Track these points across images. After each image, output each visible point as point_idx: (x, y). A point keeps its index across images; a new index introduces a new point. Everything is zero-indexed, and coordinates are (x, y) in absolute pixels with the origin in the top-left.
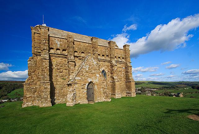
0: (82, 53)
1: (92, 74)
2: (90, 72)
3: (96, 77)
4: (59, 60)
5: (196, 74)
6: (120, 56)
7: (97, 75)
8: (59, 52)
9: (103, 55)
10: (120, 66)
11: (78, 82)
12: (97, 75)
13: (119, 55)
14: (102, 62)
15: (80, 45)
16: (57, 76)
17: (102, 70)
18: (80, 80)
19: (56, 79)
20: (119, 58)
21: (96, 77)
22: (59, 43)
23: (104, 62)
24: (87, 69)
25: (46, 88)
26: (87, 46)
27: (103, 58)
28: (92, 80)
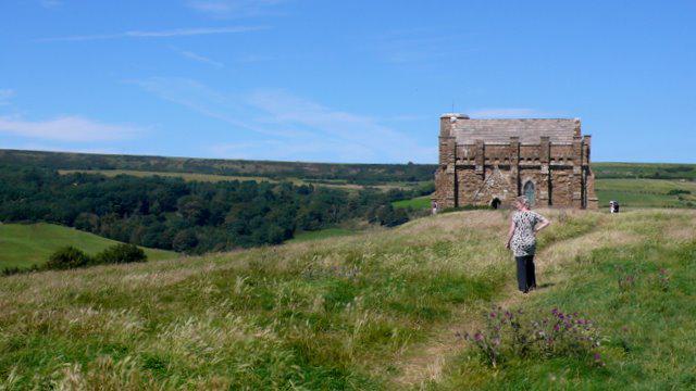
0: (496, 159)
4: (466, 171)
9: (529, 159)
27: (530, 163)
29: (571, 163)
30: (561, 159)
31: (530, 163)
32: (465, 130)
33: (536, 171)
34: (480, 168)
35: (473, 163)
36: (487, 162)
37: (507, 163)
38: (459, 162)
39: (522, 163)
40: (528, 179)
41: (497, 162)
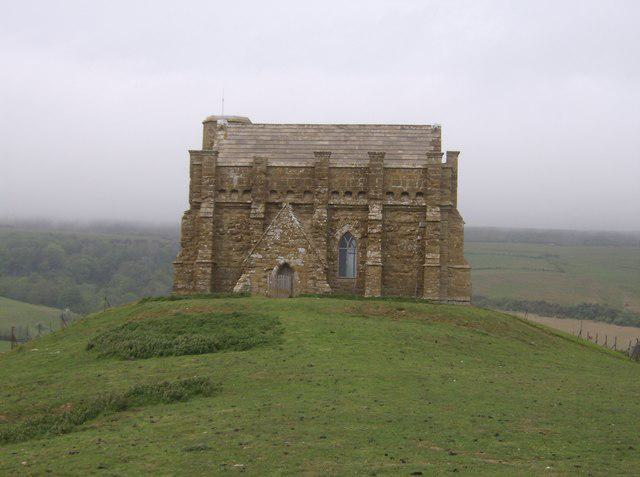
0: (289, 192)
1: (288, 247)
2: (284, 246)
3: (297, 254)
5: (5, 293)
6: (405, 190)
7: (300, 249)
8: (406, 202)
9: (348, 193)
10: (408, 217)
11: (258, 264)
12: (300, 249)
13: (404, 185)
14: (344, 212)
15: (283, 174)
16: (231, 249)
17: (344, 231)
18: (261, 260)
19: (228, 255)
20: (405, 194)
21: (297, 254)
22: (236, 177)
23: (351, 210)
24: (278, 238)
25: (204, 273)
26: (302, 175)
27: (349, 200)
28: (287, 261)
29: (421, 201)
30: (405, 194)
31: (349, 200)
32: (240, 142)
33: (359, 215)
34: (261, 209)
35: (248, 199)
36: (274, 198)
37: (307, 199)
38: (223, 198)
39: (334, 201)
40: (346, 229)
41: (290, 198)
